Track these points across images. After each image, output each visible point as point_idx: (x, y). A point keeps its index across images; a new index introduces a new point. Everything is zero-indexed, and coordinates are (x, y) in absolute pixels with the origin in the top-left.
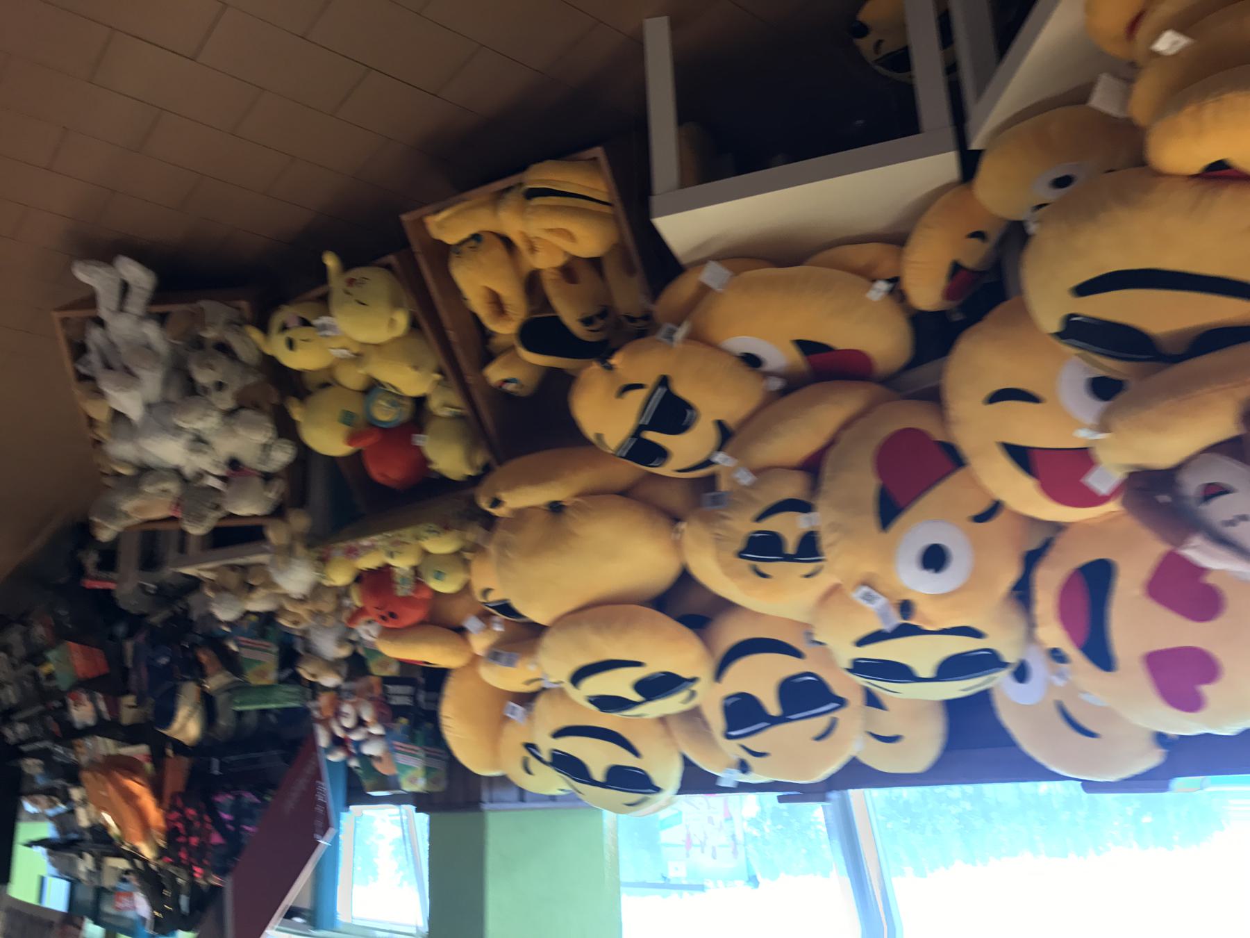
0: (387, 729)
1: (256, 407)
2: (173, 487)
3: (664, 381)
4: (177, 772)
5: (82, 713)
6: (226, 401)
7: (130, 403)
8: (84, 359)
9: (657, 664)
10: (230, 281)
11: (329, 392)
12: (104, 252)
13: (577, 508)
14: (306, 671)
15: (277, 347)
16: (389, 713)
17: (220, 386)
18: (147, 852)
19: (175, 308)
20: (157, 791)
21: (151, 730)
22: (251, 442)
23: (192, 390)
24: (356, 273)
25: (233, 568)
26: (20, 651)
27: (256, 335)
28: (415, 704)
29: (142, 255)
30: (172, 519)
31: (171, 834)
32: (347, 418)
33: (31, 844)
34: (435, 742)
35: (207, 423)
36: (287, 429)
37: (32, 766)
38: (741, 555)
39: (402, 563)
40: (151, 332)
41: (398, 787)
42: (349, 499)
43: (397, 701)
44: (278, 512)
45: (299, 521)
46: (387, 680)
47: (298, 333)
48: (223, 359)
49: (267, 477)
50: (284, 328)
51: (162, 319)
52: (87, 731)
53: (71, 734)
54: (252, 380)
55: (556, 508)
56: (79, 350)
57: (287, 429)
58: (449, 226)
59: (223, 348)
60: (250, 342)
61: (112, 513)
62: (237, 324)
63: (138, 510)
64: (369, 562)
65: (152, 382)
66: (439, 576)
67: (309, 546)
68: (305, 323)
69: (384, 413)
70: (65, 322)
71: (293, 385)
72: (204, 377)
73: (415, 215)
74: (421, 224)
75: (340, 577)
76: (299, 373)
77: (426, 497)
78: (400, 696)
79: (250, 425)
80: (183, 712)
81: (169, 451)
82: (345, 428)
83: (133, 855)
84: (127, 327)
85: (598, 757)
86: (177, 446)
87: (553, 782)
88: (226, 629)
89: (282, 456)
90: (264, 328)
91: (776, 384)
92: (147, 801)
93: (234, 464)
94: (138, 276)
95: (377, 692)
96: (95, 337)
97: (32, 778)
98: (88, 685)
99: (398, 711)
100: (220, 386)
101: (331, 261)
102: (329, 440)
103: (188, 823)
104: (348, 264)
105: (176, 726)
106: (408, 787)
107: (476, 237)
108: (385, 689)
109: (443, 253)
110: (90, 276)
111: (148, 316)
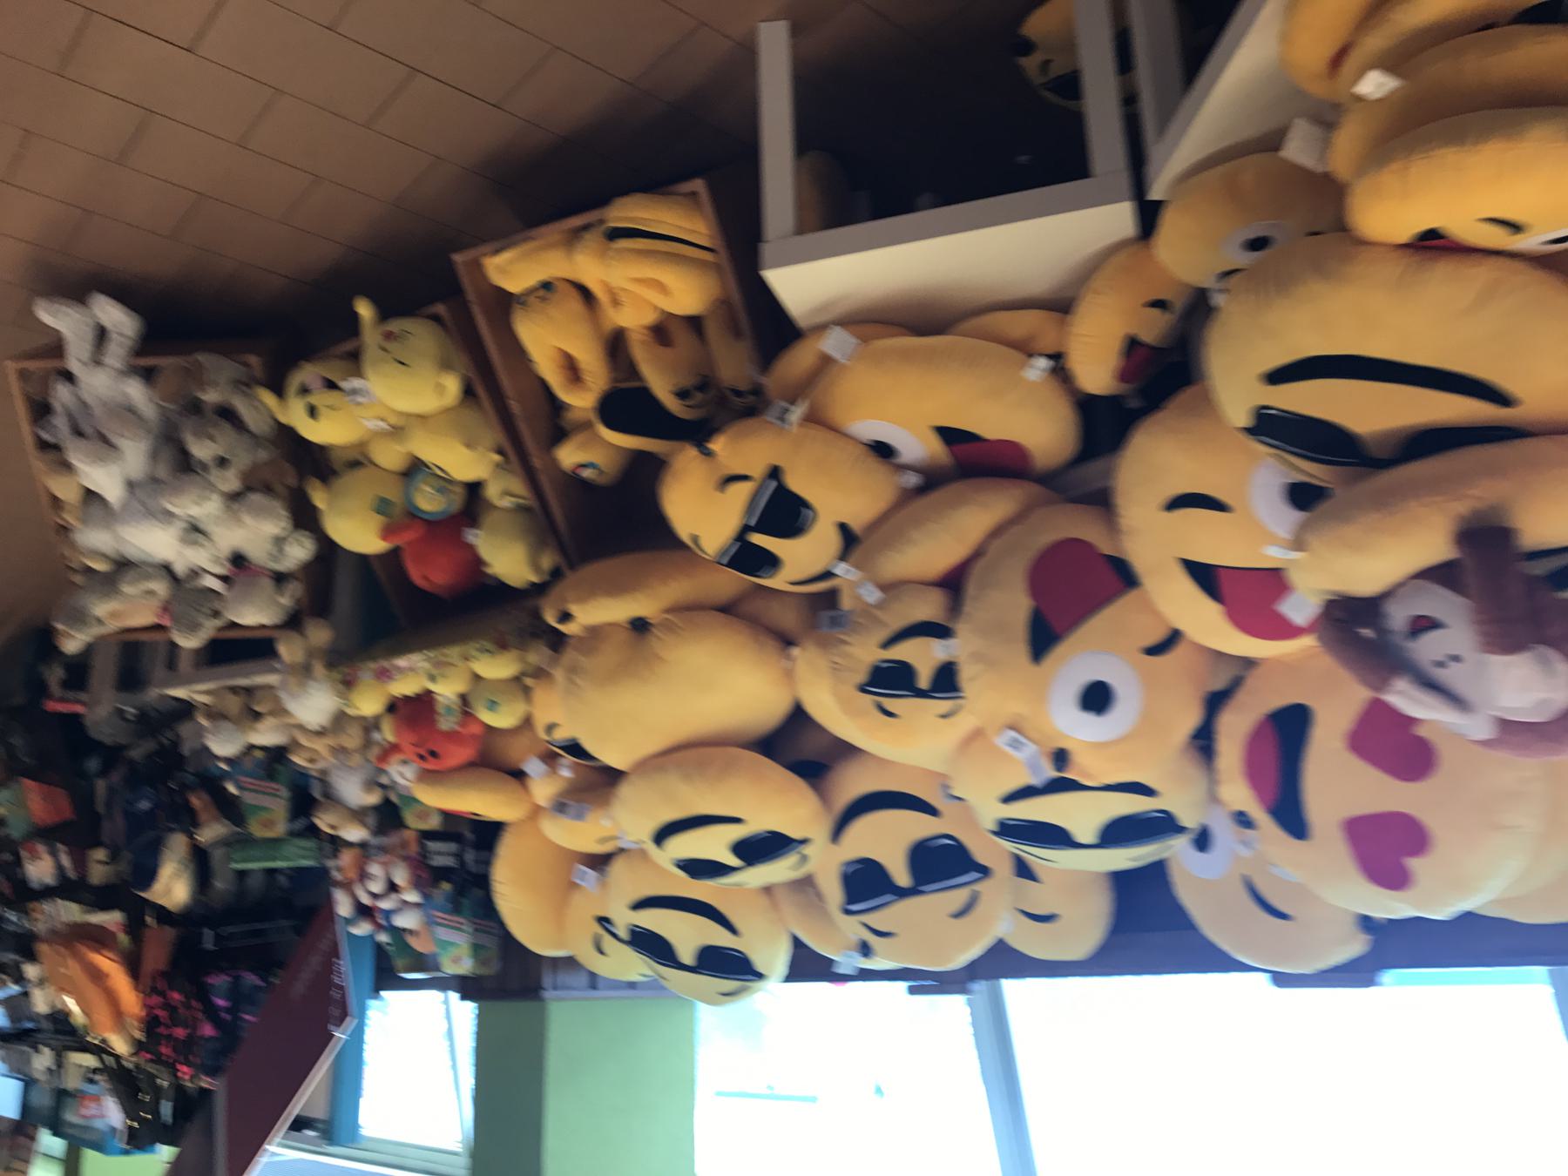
0: (426, 896)
1: (268, 489)
2: (160, 587)
5: (40, 869)
6: (230, 481)
9: (758, 822)
10: (235, 329)
11: (360, 474)
12: (75, 288)
13: (669, 627)
16: (427, 876)
17: (222, 462)
18: (120, 1045)
20: (133, 966)
21: (126, 893)
22: (261, 533)
23: (185, 465)
24: (395, 325)
25: (234, 690)
27: (268, 398)
28: (460, 865)
29: (123, 294)
30: (158, 627)
31: (151, 1024)
32: (383, 506)
35: (203, 507)
36: (305, 518)
38: (863, 689)
39: (447, 690)
40: (135, 391)
43: (439, 861)
44: (293, 622)
45: (319, 634)
46: (427, 835)
47: (321, 398)
49: (280, 578)
51: (149, 376)
52: (47, 893)
54: (263, 455)
55: (640, 626)
56: (41, 410)
57: (305, 518)
58: (512, 270)
59: (227, 414)
61: (80, 618)
62: (245, 385)
63: (114, 615)
64: (405, 687)
65: (135, 455)
66: (492, 706)
69: (429, 501)
70: (23, 375)
72: (201, 450)
74: (477, 267)
75: (368, 703)
76: (322, 449)
77: (478, 608)
78: (442, 855)
79: (259, 512)
81: (155, 541)
84: (103, 383)
85: (686, 934)
86: (161, 533)
89: (299, 551)
90: (279, 390)
91: (913, 480)
93: (239, 560)
95: (414, 849)
96: (62, 394)
98: (48, 834)
99: (441, 874)
100: (222, 462)
102: (357, 531)
107: (547, 286)
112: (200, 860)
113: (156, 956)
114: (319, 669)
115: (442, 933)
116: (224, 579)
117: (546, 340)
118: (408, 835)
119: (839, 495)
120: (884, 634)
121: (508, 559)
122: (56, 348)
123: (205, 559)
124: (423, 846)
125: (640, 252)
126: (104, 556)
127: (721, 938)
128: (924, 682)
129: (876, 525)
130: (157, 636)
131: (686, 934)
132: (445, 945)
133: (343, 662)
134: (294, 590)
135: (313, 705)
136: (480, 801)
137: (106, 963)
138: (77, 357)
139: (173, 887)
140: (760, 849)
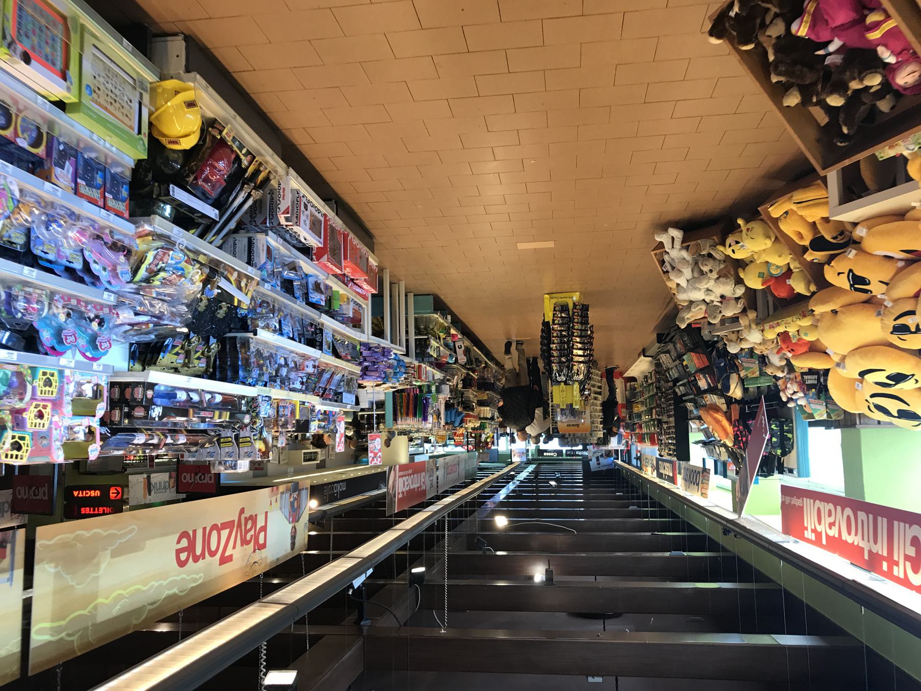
0: (805, 394)
1: (726, 276)
2: (704, 307)
3: (851, 271)
4: (735, 411)
5: (703, 384)
6: (714, 275)
7: (683, 283)
8: (665, 267)
9: (893, 370)
10: (707, 228)
11: (752, 264)
12: (664, 227)
13: (843, 313)
14: (769, 371)
15: (729, 252)
16: (806, 388)
17: (711, 271)
18: (730, 444)
19: (692, 243)
20: (729, 419)
21: (723, 391)
22: (728, 289)
23: (702, 273)
24: (750, 225)
25: (733, 332)
26: (674, 354)
27: (721, 248)
28: (818, 384)
29: (677, 225)
30: (704, 318)
31: (736, 437)
32: (761, 275)
33: (697, 443)
34: (829, 400)
35: (711, 284)
36: (739, 281)
37: (690, 406)
38: (892, 333)
39: (792, 330)
40: (684, 254)
41: (813, 418)
42: (773, 303)
43: (809, 382)
44: (744, 311)
45: (752, 315)
46: (803, 374)
47: (735, 247)
48: (711, 261)
49: (737, 299)
50: (730, 246)
51: (687, 248)
52: (705, 392)
53: (701, 393)
54: (722, 266)
55: (835, 312)
56: (662, 262)
57: (739, 281)
58: (776, 211)
59: (710, 255)
60: (722, 251)
61: (683, 320)
62: (714, 246)
63: (692, 316)
64: (781, 329)
65: (687, 272)
66: (806, 334)
67: (757, 324)
68: (737, 243)
69: (775, 272)
70: (656, 254)
71: (741, 264)
72: (705, 269)
73: (763, 207)
74: (766, 210)
75: (771, 335)
76: (742, 260)
77: (795, 304)
78: (811, 379)
79: (724, 284)
80: (732, 387)
81: (698, 295)
82: (761, 279)
83: (725, 446)
84: (676, 253)
85: (893, 406)
86: (700, 293)
87: (878, 416)
88: (276, 581)
89: (740, 291)
90: (724, 245)
91: (901, 264)
92: (725, 423)
93: (722, 297)
94: (677, 234)
95: (799, 378)
96: (666, 258)
97: (691, 411)
98: (702, 371)
99: (810, 387)
100: (711, 271)
101: (740, 222)
102: (755, 283)
103: (741, 432)
104: (747, 221)
105: (731, 392)
106: (817, 418)
107: (786, 213)
108: (803, 378)
109: (776, 221)
110: (664, 238)
111: (682, 248)
112: (742, 381)
113: (735, 415)
114: (753, 326)
115: (813, 406)
116: (721, 302)
117: (789, 228)
118: (797, 374)
119: (876, 276)
120: (894, 317)
121: (799, 287)
122: (661, 245)
123: (714, 298)
124: (803, 378)
125: (804, 207)
126: (685, 301)
127: (904, 407)
128: (913, 329)
129: (892, 279)
130: (705, 320)
131: (893, 406)
132: (816, 410)
133: (760, 322)
134: (742, 301)
135: (753, 338)
136: (818, 364)
137: (720, 417)
138: (668, 246)
139: (736, 392)
140: (899, 378)
